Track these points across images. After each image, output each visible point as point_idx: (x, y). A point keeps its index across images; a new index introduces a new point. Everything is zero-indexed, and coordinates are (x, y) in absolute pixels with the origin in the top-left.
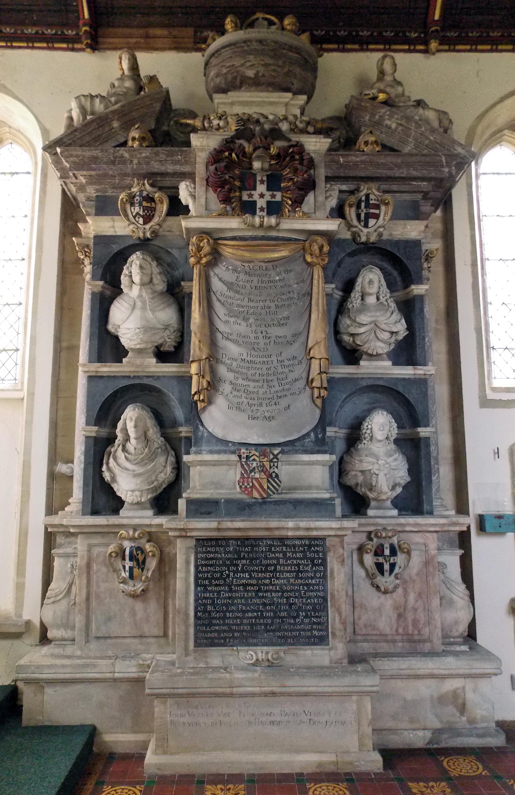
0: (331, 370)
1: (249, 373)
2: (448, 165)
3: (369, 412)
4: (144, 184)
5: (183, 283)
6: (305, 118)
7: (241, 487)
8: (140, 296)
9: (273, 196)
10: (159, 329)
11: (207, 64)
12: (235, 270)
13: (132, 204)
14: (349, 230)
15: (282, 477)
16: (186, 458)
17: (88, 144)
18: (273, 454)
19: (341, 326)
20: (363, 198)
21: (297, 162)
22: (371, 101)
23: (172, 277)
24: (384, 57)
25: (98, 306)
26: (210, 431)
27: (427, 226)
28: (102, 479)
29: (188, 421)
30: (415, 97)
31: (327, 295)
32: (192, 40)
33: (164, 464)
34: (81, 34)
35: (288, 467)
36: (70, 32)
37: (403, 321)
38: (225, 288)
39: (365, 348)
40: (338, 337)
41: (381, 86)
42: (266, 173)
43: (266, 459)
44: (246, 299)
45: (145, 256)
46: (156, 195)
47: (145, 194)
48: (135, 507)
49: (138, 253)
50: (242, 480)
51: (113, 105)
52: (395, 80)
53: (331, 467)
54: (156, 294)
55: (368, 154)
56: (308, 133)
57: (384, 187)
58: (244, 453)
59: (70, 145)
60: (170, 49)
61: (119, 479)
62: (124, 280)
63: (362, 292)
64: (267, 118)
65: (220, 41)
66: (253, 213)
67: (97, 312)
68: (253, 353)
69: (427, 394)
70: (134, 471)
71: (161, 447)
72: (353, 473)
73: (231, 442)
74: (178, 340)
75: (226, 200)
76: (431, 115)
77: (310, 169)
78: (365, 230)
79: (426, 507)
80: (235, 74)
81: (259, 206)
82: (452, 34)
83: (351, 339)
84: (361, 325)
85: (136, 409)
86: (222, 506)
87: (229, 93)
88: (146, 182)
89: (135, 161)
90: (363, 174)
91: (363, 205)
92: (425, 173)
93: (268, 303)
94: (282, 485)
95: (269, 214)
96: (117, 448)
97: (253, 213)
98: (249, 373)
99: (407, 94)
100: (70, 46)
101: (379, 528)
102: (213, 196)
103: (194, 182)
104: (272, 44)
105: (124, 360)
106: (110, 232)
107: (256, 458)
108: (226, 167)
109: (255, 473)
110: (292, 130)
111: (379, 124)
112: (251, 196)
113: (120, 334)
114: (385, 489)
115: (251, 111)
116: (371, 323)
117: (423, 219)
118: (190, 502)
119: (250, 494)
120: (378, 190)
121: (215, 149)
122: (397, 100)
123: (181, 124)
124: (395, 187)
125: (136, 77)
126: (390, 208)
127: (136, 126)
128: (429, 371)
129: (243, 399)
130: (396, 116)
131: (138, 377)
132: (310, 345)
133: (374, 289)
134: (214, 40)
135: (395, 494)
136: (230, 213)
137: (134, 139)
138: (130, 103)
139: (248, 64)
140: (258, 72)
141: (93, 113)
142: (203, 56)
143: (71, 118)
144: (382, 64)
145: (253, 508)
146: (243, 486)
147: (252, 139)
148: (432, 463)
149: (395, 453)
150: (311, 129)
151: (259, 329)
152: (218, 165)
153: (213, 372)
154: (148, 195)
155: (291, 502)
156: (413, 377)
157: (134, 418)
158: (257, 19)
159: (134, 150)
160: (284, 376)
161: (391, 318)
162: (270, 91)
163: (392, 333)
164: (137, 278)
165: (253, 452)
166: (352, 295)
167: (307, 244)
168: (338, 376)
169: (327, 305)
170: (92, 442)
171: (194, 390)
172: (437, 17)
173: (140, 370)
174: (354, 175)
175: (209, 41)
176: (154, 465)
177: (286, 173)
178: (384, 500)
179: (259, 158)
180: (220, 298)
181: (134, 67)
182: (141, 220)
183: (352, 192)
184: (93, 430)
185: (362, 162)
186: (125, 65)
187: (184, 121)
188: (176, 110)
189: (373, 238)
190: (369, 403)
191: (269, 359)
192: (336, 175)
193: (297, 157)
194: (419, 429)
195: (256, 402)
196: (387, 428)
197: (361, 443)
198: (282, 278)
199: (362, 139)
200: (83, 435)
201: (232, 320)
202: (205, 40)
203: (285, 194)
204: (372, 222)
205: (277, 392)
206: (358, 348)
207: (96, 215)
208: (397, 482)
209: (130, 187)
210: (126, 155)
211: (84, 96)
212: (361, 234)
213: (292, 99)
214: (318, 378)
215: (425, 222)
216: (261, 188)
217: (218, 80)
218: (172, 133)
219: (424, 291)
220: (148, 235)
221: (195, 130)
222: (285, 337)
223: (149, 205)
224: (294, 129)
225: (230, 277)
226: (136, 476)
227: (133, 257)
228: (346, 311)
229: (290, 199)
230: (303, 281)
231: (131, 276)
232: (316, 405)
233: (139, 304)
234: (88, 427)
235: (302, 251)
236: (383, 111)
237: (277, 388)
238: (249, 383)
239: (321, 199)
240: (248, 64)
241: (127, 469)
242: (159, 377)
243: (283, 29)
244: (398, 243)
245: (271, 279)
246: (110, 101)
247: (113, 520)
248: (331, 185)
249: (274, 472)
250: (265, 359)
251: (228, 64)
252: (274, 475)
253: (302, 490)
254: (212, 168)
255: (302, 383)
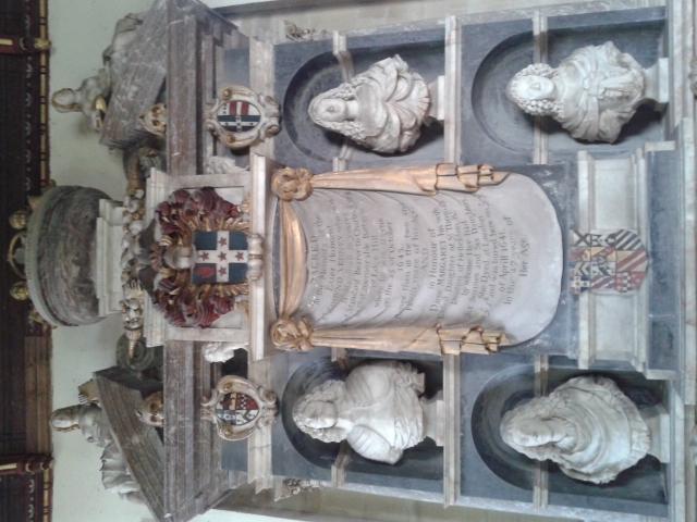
0: (451, 160)
1: (458, 274)
2: (180, 16)
3: (508, 101)
4: (209, 408)
5: (334, 360)
6: (127, 201)
7: (630, 289)
8: (351, 418)
9: (223, 242)
10: (395, 395)
11: (65, 323)
12: (318, 292)
13: (233, 423)
14: (263, 141)
15: (613, 228)
16: (583, 366)
17: (160, 475)
18: (579, 242)
19: (389, 147)
20: (223, 123)
21: (180, 211)
22: (106, 118)
23: (324, 372)
24: (55, 104)
25: (366, 476)
26: (541, 329)
27: (256, 38)
28: (611, 484)
29: (526, 358)
30: (99, 62)
31: (347, 168)
32: (38, 338)
33: (589, 395)
34: (33, 473)
35: (598, 219)
36: (31, 511)
37: (382, 63)
38: (342, 304)
39: (420, 115)
40: (404, 150)
41: (87, 106)
42: (195, 252)
43: (586, 252)
44: (357, 277)
45: (300, 410)
46: (221, 391)
47: (220, 407)
48: (655, 439)
49: (295, 419)
50: (619, 287)
51: (113, 442)
52: (80, 90)
53: (595, 156)
54: (348, 396)
55: (169, 120)
56: (144, 196)
57: (207, 97)
58: (578, 284)
59: (161, 499)
60: (48, 365)
61: (613, 460)
62: (329, 438)
63: (343, 121)
64: (127, 250)
65: (39, 307)
66: (244, 267)
67: (374, 477)
68: (430, 268)
69: (485, 25)
70: (601, 440)
71: (565, 398)
72: (602, 124)
73: (560, 301)
74: (410, 368)
75: (228, 303)
76: (121, 42)
77: (188, 194)
78: (264, 119)
79: (654, 17)
80: (76, 289)
81: (235, 261)
82: (28, 22)
83: (407, 133)
84: (388, 121)
85: (510, 431)
86: (659, 316)
87: (98, 297)
88: (206, 405)
89: (180, 418)
90: (193, 126)
91: (231, 124)
92: (191, 46)
93: (361, 248)
94: (626, 228)
95: (245, 247)
96: (566, 463)
97: (244, 267)
98: (458, 274)
99: (96, 73)
100: (46, 486)
101: (688, 85)
102: (222, 320)
103: (206, 343)
104: (42, 244)
105: (439, 443)
106: (268, 453)
107: (585, 266)
108: (187, 303)
109: (608, 268)
110: (141, 218)
111: (131, 107)
112: (223, 271)
113: (403, 447)
114: (627, 78)
115: (119, 268)
116: (385, 107)
117: (248, 43)
118: (653, 363)
119: (641, 275)
120: (212, 105)
121: (166, 317)
122: (104, 87)
123: (135, 356)
124: (208, 84)
125: (82, 410)
126: (236, 87)
127: (138, 415)
128: (451, 24)
129: (496, 282)
130: (123, 86)
131: (463, 425)
132: (418, 191)
133: (339, 105)
134: (38, 314)
135: (634, 64)
136: (244, 297)
137: (153, 419)
138: (111, 421)
139: (65, 274)
140: (74, 261)
141: (124, 468)
142: (55, 327)
143: (130, 494)
144: (62, 106)
145: (662, 271)
146: (629, 285)
147: (152, 270)
148: (584, 12)
149: (571, 65)
150: (139, 194)
151: (397, 260)
152: (185, 314)
153: (456, 323)
154: (221, 403)
155: (654, 216)
156: (460, 46)
157: (523, 436)
158: (14, 260)
159: (168, 420)
160: (462, 226)
161: (379, 79)
162: (96, 246)
163: (399, 77)
164: (329, 422)
165: (576, 270)
166: (347, 134)
167: (283, 196)
168: (459, 150)
169: (361, 168)
170: (556, 496)
171: (481, 350)
172: (9, 42)
173: (452, 423)
174: (194, 137)
175: (39, 320)
176: (592, 410)
177: (194, 226)
178: (644, 80)
179: (175, 260)
180: (354, 312)
181: (70, 412)
182: (253, 412)
183: (216, 139)
184: (540, 493)
185: (178, 127)
186: (67, 423)
187: (131, 353)
188: (118, 362)
189: (274, 109)
190: (497, 102)
191: (438, 247)
192: (195, 160)
193: (174, 212)
194: (536, 32)
195: (500, 265)
196: (536, 78)
197: (557, 114)
198: (327, 230)
199: (151, 129)
200: (546, 507)
201: (384, 296)
202: (38, 326)
203: (220, 227)
204: (252, 111)
205: (485, 235)
206: (419, 123)
207: (246, 470)
208: (615, 60)
209: (212, 425)
210: (173, 429)
211: (103, 478)
212: (269, 124)
213: (104, 218)
214: (464, 180)
215: (252, 40)
216: (213, 257)
217: (84, 310)
218: (145, 367)
219: (341, 38)
220: (271, 403)
221: (142, 341)
222: (407, 225)
223: (234, 401)
224: (140, 214)
225: (327, 298)
226: (608, 436)
227: (300, 425)
228: (369, 142)
229: (226, 219)
230: (331, 201)
231: (325, 429)
232: (503, 180)
233: (362, 420)
234: (535, 500)
235: (293, 203)
236: (116, 102)
237: (479, 235)
238: (472, 275)
239: (225, 180)
240: (65, 274)
241: (599, 449)
242: (462, 397)
243: (24, 229)
244: (279, 76)
245: (329, 243)
246: (109, 445)
247: (677, 473)
248: (207, 166)
249: (606, 240)
250: (439, 252)
251: (65, 299)
252: (611, 241)
253: (632, 199)
254: (189, 321)
255: (469, 198)
